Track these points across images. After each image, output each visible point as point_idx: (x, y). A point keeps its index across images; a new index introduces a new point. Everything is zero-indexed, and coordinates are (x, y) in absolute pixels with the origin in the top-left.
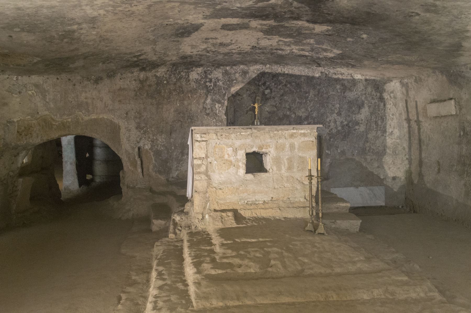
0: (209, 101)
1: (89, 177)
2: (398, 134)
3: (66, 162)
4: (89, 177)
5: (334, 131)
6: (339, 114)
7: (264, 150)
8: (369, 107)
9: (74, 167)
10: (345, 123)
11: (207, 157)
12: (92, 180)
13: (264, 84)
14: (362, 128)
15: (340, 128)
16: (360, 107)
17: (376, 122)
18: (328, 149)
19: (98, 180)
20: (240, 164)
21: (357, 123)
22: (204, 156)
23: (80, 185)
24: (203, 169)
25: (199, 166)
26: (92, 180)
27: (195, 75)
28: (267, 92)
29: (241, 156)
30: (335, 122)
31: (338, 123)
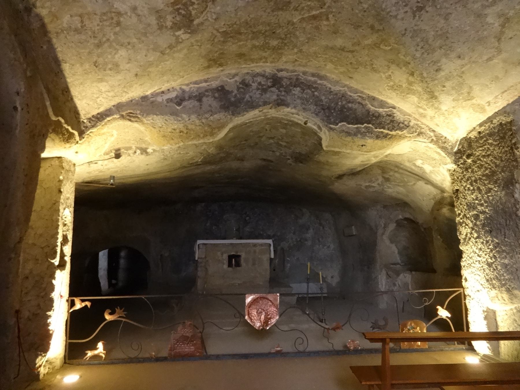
0: (208, 224)
1: (114, 282)
2: (333, 247)
3: (101, 269)
4: (114, 282)
5: (292, 245)
6: (294, 233)
7: (239, 254)
8: (313, 229)
9: (106, 273)
10: (298, 240)
11: (206, 257)
12: (117, 284)
13: (246, 213)
14: (309, 243)
15: (295, 243)
16: (308, 229)
17: (318, 239)
18: (288, 257)
19: (120, 284)
20: (225, 262)
21: (306, 240)
22: (203, 257)
23: (109, 287)
24: (203, 264)
25: (201, 263)
26: (117, 284)
27: (200, 207)
28: (248, 218)
29: (225, 256)
30: (292, 239)
31: (294, 240)
